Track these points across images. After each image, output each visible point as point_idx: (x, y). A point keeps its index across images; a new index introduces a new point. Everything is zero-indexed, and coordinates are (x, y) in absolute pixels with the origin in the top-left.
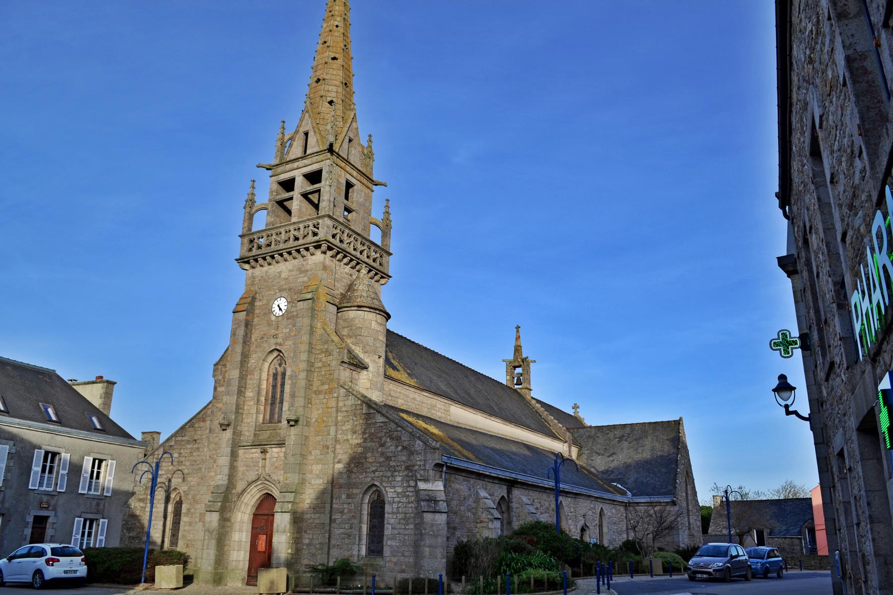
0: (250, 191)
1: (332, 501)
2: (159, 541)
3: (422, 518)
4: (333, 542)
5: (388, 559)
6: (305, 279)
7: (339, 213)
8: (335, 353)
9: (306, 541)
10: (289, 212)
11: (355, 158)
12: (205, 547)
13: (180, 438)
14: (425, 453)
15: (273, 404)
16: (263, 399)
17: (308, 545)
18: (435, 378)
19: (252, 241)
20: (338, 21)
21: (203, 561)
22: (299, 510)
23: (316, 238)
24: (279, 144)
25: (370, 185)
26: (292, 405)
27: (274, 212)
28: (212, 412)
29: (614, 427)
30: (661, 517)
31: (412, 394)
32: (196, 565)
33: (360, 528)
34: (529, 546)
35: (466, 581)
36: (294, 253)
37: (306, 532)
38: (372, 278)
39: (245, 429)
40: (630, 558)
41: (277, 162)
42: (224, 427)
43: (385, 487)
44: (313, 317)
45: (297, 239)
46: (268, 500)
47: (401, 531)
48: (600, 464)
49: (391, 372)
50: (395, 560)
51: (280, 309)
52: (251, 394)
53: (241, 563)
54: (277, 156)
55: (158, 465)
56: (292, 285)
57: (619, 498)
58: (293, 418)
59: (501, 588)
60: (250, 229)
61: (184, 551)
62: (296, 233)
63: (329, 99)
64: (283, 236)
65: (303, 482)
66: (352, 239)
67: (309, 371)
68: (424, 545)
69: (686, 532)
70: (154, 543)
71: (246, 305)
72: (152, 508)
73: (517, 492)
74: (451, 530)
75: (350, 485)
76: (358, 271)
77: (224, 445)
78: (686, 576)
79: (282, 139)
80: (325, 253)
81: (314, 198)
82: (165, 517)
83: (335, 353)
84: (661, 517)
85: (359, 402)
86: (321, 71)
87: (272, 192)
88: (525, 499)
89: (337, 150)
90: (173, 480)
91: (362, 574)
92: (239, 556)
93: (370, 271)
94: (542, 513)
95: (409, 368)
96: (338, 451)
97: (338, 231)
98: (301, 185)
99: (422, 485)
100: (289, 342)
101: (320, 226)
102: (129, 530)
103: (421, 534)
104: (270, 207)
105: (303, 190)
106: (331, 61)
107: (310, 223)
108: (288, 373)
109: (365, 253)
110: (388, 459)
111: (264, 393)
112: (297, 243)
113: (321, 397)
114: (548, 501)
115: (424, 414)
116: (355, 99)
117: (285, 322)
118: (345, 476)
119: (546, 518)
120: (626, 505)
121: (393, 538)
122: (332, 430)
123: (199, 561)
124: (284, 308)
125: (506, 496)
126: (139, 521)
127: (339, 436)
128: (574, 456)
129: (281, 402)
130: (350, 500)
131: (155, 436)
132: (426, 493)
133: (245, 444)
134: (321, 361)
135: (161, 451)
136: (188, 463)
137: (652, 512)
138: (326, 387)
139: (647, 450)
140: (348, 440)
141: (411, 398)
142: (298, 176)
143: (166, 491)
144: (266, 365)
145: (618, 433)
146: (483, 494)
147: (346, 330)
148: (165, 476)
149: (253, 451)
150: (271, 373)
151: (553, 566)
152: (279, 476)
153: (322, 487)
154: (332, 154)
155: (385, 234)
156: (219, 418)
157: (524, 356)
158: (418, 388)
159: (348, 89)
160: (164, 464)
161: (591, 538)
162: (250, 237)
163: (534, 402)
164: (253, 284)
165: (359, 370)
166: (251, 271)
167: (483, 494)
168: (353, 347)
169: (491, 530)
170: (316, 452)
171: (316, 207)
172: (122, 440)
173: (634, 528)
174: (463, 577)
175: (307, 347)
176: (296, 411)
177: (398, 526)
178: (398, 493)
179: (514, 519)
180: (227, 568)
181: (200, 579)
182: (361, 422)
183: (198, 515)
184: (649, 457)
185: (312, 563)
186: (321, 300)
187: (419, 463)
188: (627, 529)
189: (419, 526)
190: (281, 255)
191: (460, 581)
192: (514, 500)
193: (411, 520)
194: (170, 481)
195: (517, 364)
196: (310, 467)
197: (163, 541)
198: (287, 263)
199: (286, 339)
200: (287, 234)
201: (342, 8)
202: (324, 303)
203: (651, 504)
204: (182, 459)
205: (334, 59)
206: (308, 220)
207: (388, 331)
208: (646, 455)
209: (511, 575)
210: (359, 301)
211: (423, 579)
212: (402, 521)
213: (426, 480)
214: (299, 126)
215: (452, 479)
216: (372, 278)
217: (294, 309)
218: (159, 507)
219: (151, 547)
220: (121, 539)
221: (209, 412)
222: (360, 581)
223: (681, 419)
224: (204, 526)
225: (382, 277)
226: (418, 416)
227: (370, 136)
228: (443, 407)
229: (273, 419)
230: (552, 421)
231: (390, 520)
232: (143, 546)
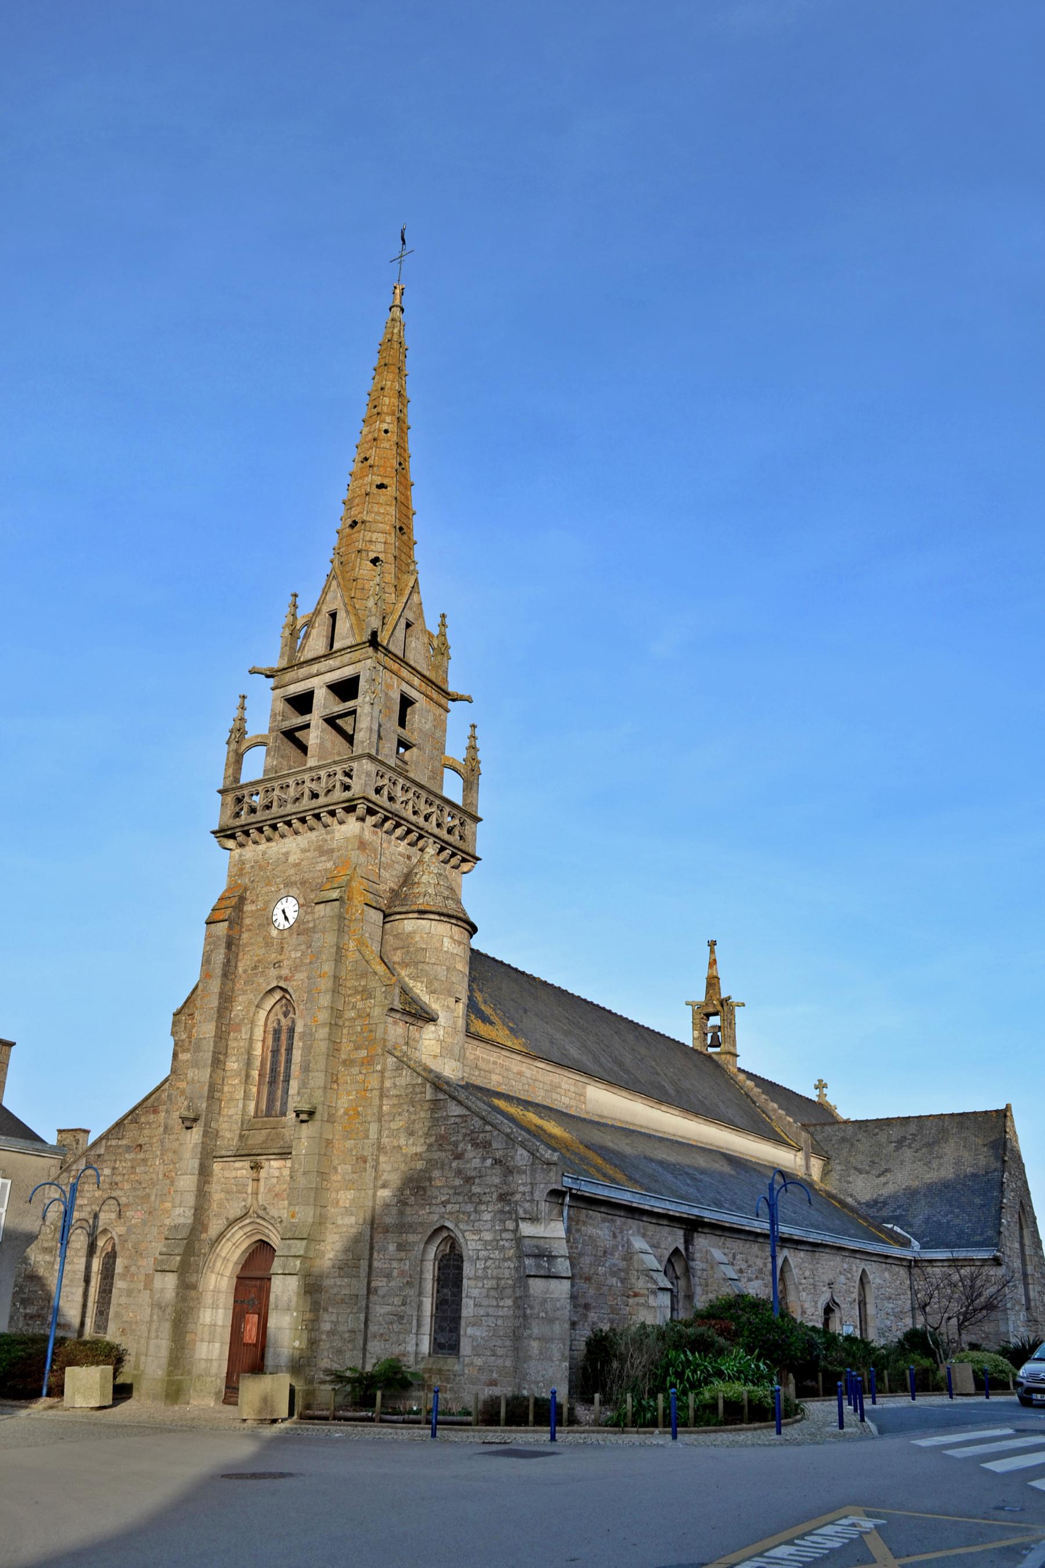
0: (236, 713)
1: (371, 1255)
2: (76, 1322)
3: (526, 1287)
4: (373, 1328)
5: (467, 1360)
6: (329, 865)
7: (388, 751)
8: (379, 994)
9: (327, 1327)
10: (303, 748)
11: (417, 655)
12: (153, 1335)
13: (114, 1142)
14: (533, 1171)
15: (273, 1082)
16: (255, 1074)
17: (331, 1333)
18: (558, 1036)
19: (239, 800)
20: (388, 422)
21: (149, 1363)
22: (315, 1271)
23: (347, 795)
24: (287, 632)
25: (443, 701)
26: (304, 1085)
27: (278, 749)
28: (169, 1096)
29: (888, 1122)
30: (972, 1287)
31: (516, 1064)
32: (137, 1367)
33: (420, 1306)
34: (721, 1340)
35: (602, 1403)
37: (326, 1310)
38: (446, 862)
39: (225, 1126)
40: (916, 1364)
41: (284, 664)
42: (189, 1122)
43: (463, 1232)
44: (341, 931)
45: (315, 796)
46: (261, 1251)
47: (491, 1311)
48: (862, 1189)
49: (479, 1027)
50: (479, 1361)
51: (286, 918)
52: (235, 1066)
53: (215, 1364)
55: (74, 1188)
56: (307, 876)
57: (896, 1251)
58: (306, 1107)
59: (665, 1415)
60: (237, 780)
61: (117, 1341)
62: (314, 786)
63: (372, 555)
64: (292, 792)
65: (321, 1221)
66: (410, 795)
67: (335, 1024)
68: (530, 1336)
69: (1023, 1315)
70: (66, 1326)
71: (229, 911)
72: (63, 1264)
73: (702, 1242)
74: (581, 1310)
75: (402, 1228)
76: (422, 850)
77: (187, 1155)
78: (1016, 1398)
79: (293, 624)
80: (362, 819)
81: (346, 724)
82: (87, 1281)
83: (379, 994)
84: (972, 1287)
85: (420, 1081)
86: (359, 509)
87: (274, 715)
88: (718, 1254)
89: (385, 644)
90: (102, 1216)
91: (421, 1387)
92: (211, 1352)
93: (442, 849)
94: (750, 1280)
95: (513, 1020)
96: (383, 1166)
97: (386, 781)
98: (324, 703)
99: (527, 1229)
100: (301, 976)
101: (354, 773)
102: (25, 1302)
103: (525, 1316)
104: (271, 742)
105: (328, 711)
106: (375, 490)
107: (338, 769)
108: (299, 1029)
109: (433, 819)
110: (469, 1180)
111: (257, 1063)
112: (315, 803)
113: (355, 1070)
114: (758, 1256)
115: (538, 1100)
116: (418, 553)
117: (294, 940)
118: (394, 1211)
119: (757, 1289)
120: (912, 1265)
121: (476, 1323)
122: (373, 1128)
123: (143, 1358)
124: (292, 916)
125: (682, 1248)
126: (43, 1286)
127: (385, 1140)
128: (816, 1174)
129: (287, 1080)
130: (403, 1254)
131: (80, 1136)
132: (535, 1242)
133: (224, 1153)
134: (354, 1007)
135: (82, 1164)
136: (127, 1186)
137: (956, 1277)
138: (363, 1053)
139: (952, 1162)
140: (400, 1147)
141: (511, 1072)
142: (319, 686)
143: (89, 1235)
144: (262, 1014)
145: (895, 1133)
146: (639, 1244)
147: (399, 952)
148: (88, 1209)
149: (238, 1165)
150: (270, 1029)
151: (762, 1377)
152: (280, 1210)
153: (354, 1230)
154: (376, 649)
155: (470, 785)
156: (181, 1107)
157: (724, 996)
158: (527, 1055)
159: (405, 537)
160: (86, 1187)
161: (845, 1326)
162: (234, 792)
163: (742, 1077)
164: (241, 873)
165: (420, 1023)
166: (238, 851)
167: (639, 1244)
168: (411, 983)
169: (654, 1311)
170: (344, 1169)
171: (350, 739)
172: (22, 1143)
173: (923, 1307)
174: (597, 1396)
175: (330, 984)
176: (311, 1096)
177: (485, 1302)
178: (486, 1243)
179: (698, 1290)
180: (189, 1373)
181: (143, 1391)
182: (423, 1114)
183: (142, 1277)
184: (951, 1176)
185: (336, 1366)
186: (356, 902)
187: (521, 1189)
188: (913, 1309)
189: (522, 1301)
190: (289, 824)
191: (591, 1402)
192: (697, 1255)
193: (509, 1291)
194: (96, 1216)
195: (711, 1010)
196: (334, 1195)
197: (82, 1324)
199: (296, 968)
200: (300, 788)
201: (395, 401)
202: (361, 906)
203: (953, 1262)
204: (118, 1179)
205: (381, 486)
206: (335, 763)
207: (472, 950)
208: (947, 1173)
209: (685, 1393)
210: (421, 903)
211: (526, 1399)
212: (493, 1293)
213: (534, 1219)
215: (583, 1217)
216: (446, 862)
217: (309, 917)
218: (77, 1263)
219: (61, 1333)
220: (11, 1318)
221: (164, 1096)
222: (418, 1399)
223: (1008, 1107)
224: (151, 1297)
225: (464, 860)
226: (527, 1104)
227: (443, 616)
228: (572, 1089)
229: (272, 1108)
230: (774, 1110)
231: (472, 1290)
232: (48, 1331)
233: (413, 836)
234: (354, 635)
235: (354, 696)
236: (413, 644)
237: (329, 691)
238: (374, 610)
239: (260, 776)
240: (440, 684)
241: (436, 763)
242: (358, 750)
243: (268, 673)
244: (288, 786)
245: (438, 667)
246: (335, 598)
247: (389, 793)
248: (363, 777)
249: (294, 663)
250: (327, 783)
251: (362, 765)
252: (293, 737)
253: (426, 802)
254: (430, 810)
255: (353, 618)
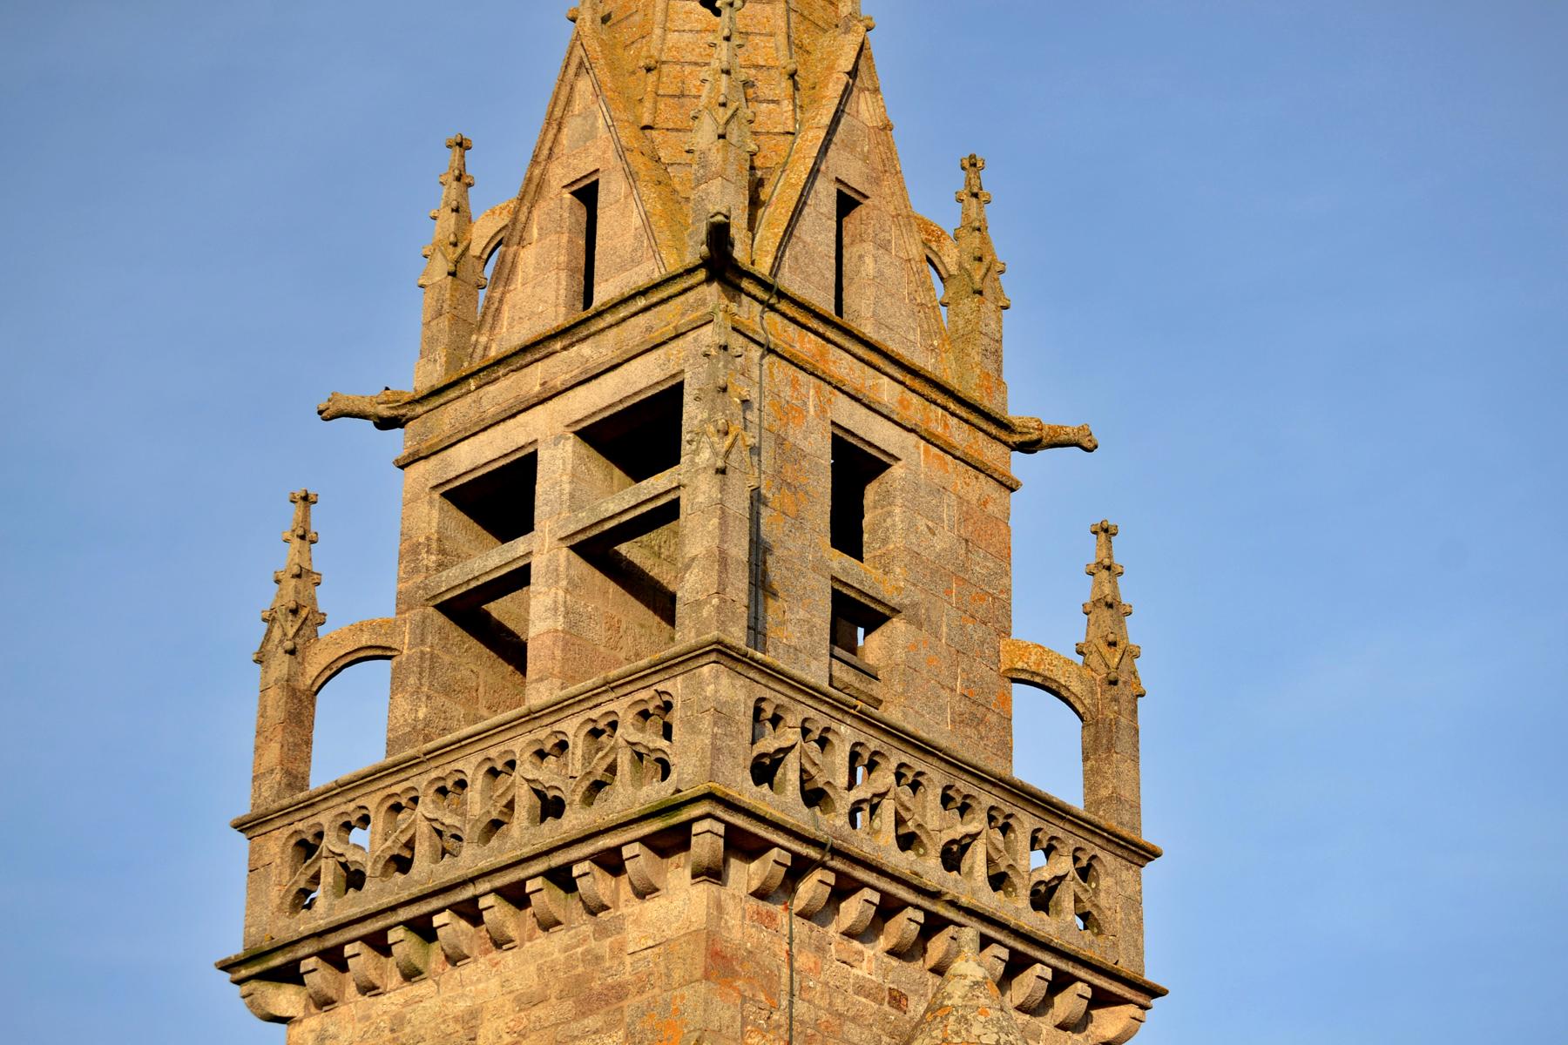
0: (287, 556)
7: (799, 632)
19: (307, 849)
23: (656, 792)
24: (439, 269)
25: (992, 453)
36: (544, 896)
38: (1034, 1009)
41: (434, 374)
45: (551, 807)
54: (431, 342)
60: (296, 780)
62: (548, 774)
64: (477, 803)
66: (884, 778)
76: (939, 970)
80: (713, 873)
87: (411, 552)
89: (763, 267)
97: (790, 736)
98: (575, 492)
105: (585, 518)
109: (976, 859)
155: (1107, 732)
162: (291, 821)
166: (314, 1022)
190: (470, 912)
198: (508, 957)
206: (610, 686)
214: (543, 156)
216: (1034, 1009)
225: (1101, 999)
233: (905, 925)
234: (656, 253)
235: (668, 455)
236: (869, 266)
237: (585, 450)
238: (716, 157)
239: (376, 756)
240: (975, 395)
241: (981, 669)
242: (687, 635)
243: (384, 411)
244: (462, 784)
245: (966, 339)
246: (591, 135)
247: (900, 821)
248: (706, 723)
249: (466, 367)
250: (587, 758)
251: (701, 685)
252: (475, 614)
253: (946, 800)
254: (960, 830)
255: (649, 193)
